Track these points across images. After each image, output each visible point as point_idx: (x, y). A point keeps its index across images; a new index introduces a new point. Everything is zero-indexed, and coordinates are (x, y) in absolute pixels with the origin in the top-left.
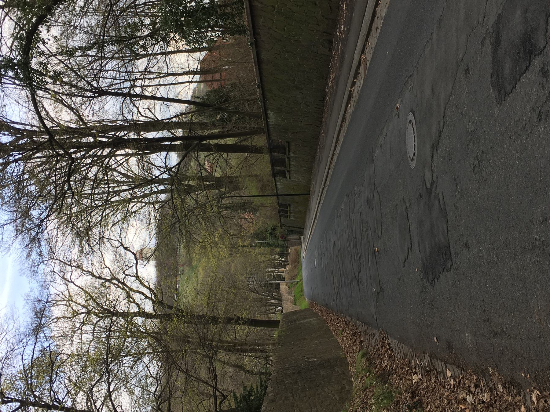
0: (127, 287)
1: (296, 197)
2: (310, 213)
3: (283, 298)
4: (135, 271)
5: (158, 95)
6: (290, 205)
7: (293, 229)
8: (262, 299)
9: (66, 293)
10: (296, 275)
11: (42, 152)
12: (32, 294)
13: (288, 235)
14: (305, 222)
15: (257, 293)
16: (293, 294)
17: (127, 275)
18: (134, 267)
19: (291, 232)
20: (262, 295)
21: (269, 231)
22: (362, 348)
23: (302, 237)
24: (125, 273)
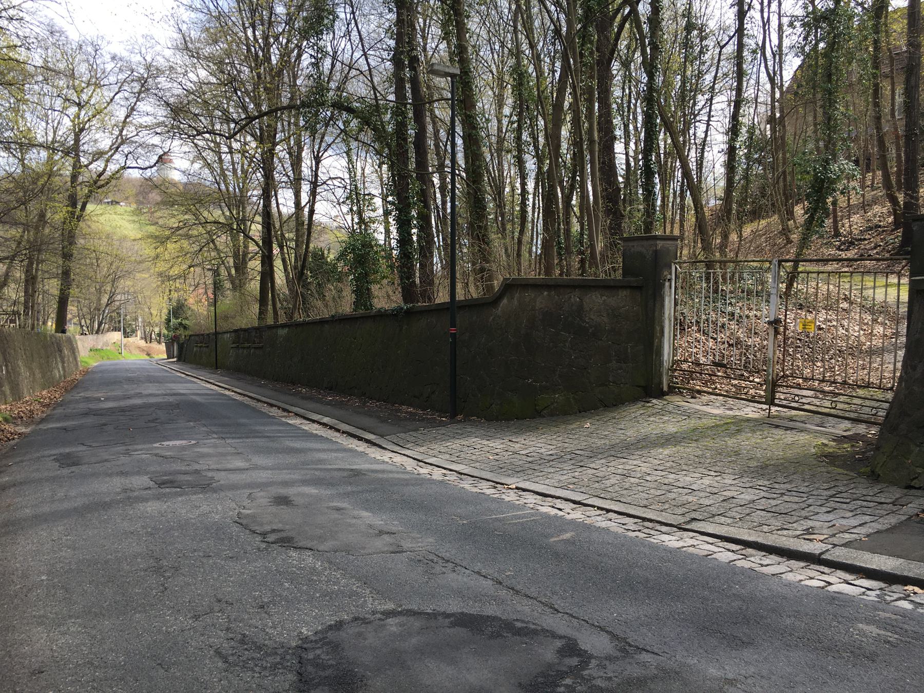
0: (112, 156)
1: (213, 354)
2: (196, 369)
3: (100, 336)
4: (131, 166)
5: (149, 169)
6: (208, 347)
7: (184, 349)
8: (99, 310)
9: (106, 82)
10: (131, 352)
11: (615, 138)
12: (105, 43)
13: (178, 343)
14: (191, 363)
15: (107, 305)
16: (104, 348)
17: (127, 156)
18: (136, 165)
19: (181, 348)
20: (104, 311)
21: (183, 322)
22: (15, 418)
23: (175, 359)
24: (130, 155)
